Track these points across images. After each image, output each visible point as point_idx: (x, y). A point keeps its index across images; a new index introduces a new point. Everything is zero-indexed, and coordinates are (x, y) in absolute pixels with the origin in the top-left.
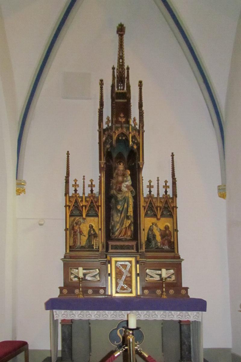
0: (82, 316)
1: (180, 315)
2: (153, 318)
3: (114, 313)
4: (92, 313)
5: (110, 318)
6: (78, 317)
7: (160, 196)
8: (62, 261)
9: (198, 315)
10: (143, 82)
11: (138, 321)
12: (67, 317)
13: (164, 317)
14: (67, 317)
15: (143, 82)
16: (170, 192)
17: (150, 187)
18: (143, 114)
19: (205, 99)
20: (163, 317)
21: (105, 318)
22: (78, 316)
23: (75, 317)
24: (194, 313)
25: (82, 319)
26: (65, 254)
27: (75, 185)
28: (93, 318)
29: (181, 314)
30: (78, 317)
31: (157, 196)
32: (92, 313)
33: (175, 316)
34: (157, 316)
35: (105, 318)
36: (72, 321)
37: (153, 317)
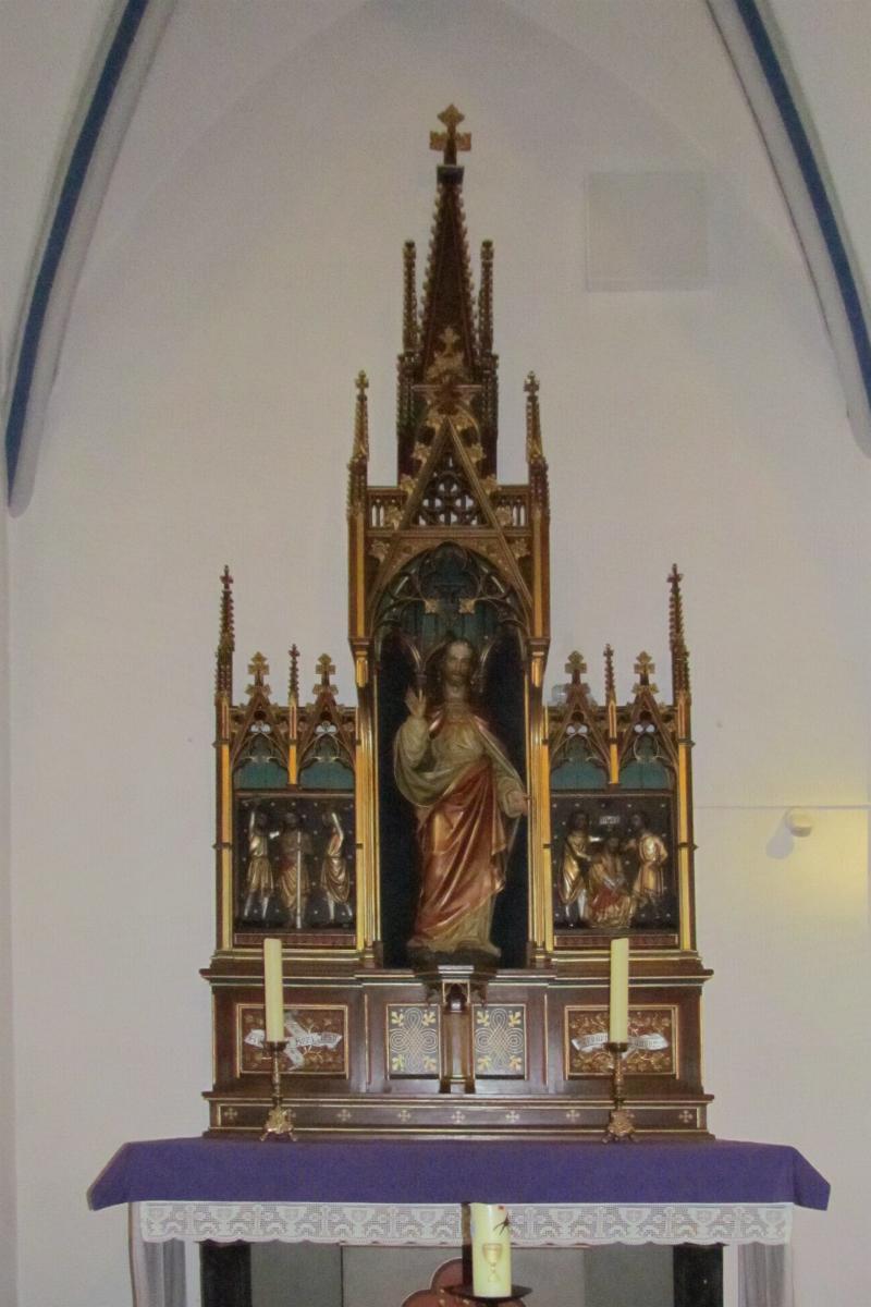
0: (588, 1232)
1: (242, 1221)
2: (265, 1233)
3: (242, 1212)
4: (219, 1216)
5: (295, 1233)
6: (163, 1230)
7: (617, 700)
8: (207, 982)
9: (657, 1219)
10: (495, 246)
11: (521, 1256)
12: (592, 1236)
13: (246, 1229)
14: (592, 1236)
15: (494, 246)
16: (662, 681)
17: (576, 666)
18: (494, 372)
19: (115, 159)
20: (581, 1232)
21: (617, 1238)
22: (435, 1231)
23: (766, 1233)
24: (710, 1213)
25: (656, 1241)
26: (217, 954)
27: (259, 666)
28: (357, 1236)
29: (588, 1219)
30: (296, 1231)
31: (608, 702)
32: (422, 1219)
33: (652, 1224)
34: (764, 1230)
35: (613, 1235)
36: (341, 1250)
37: (405, 1231)
